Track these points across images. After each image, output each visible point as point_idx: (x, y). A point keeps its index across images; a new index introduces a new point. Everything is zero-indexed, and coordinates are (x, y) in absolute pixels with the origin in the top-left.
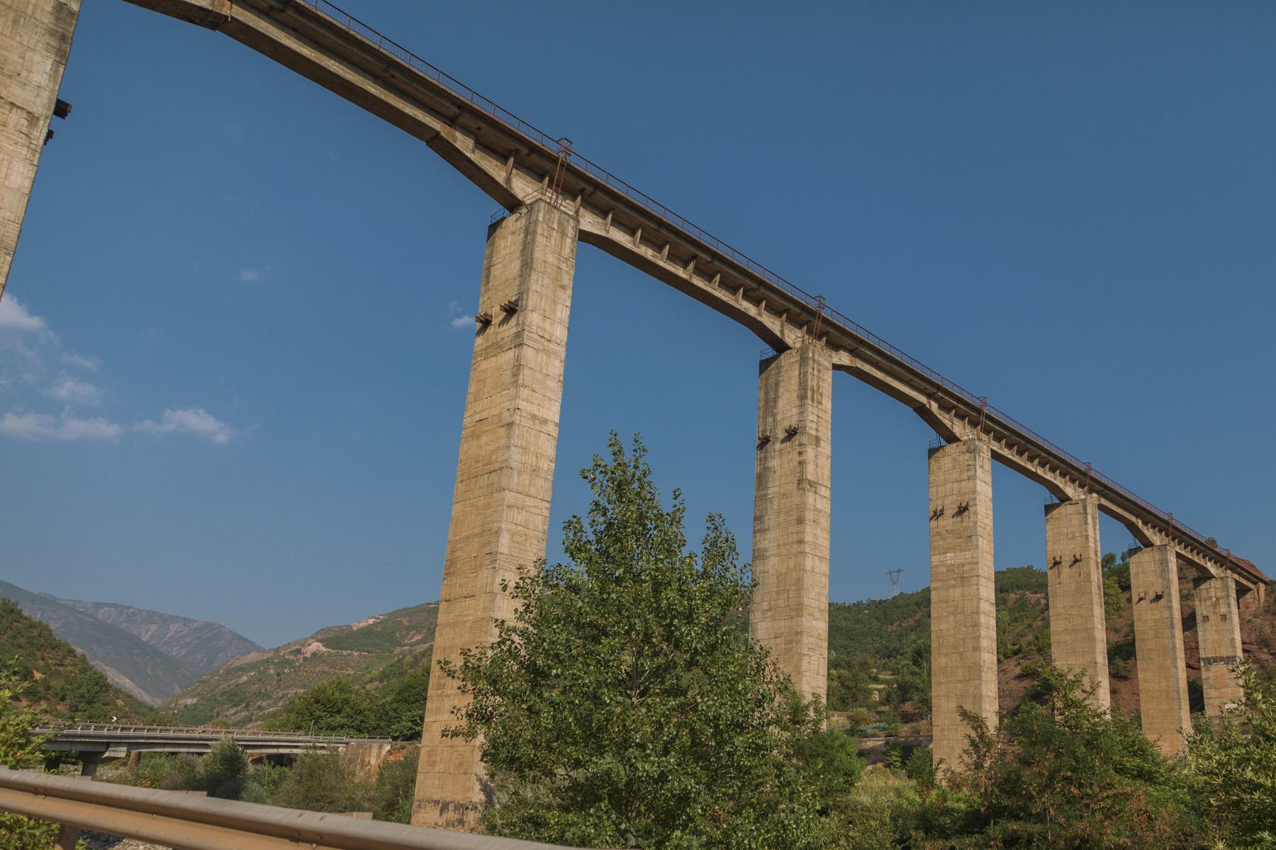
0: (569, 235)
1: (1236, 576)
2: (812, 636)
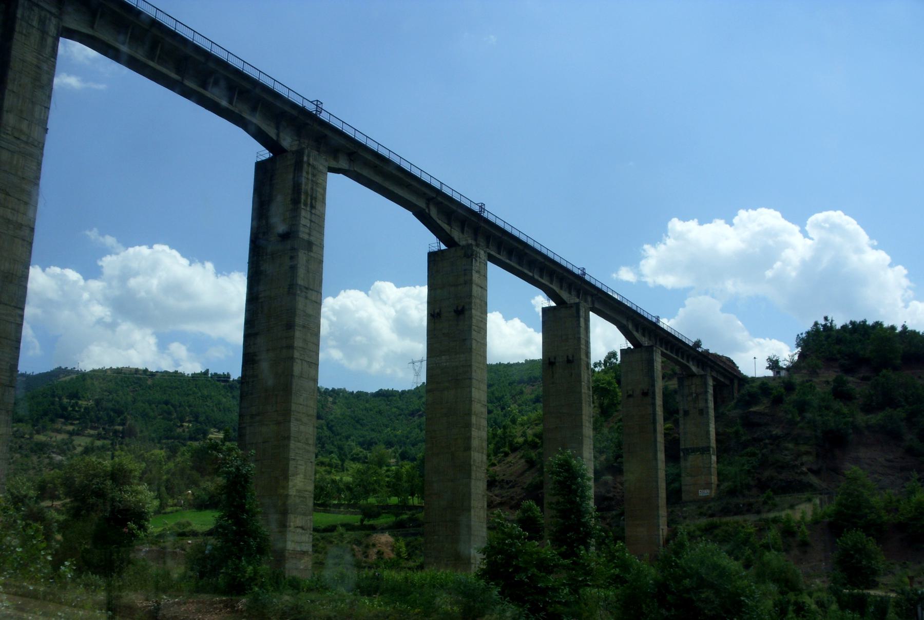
0: (51, 33)
1: (714, 374)
2: (299, 441)
